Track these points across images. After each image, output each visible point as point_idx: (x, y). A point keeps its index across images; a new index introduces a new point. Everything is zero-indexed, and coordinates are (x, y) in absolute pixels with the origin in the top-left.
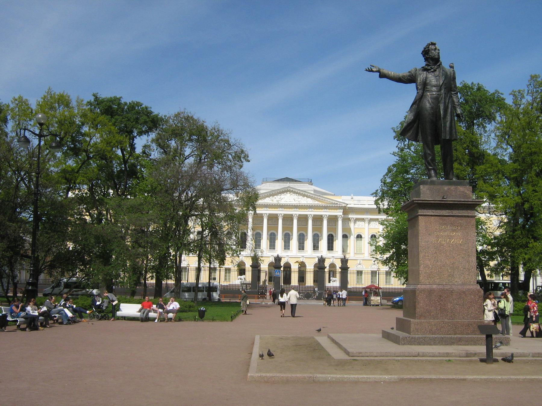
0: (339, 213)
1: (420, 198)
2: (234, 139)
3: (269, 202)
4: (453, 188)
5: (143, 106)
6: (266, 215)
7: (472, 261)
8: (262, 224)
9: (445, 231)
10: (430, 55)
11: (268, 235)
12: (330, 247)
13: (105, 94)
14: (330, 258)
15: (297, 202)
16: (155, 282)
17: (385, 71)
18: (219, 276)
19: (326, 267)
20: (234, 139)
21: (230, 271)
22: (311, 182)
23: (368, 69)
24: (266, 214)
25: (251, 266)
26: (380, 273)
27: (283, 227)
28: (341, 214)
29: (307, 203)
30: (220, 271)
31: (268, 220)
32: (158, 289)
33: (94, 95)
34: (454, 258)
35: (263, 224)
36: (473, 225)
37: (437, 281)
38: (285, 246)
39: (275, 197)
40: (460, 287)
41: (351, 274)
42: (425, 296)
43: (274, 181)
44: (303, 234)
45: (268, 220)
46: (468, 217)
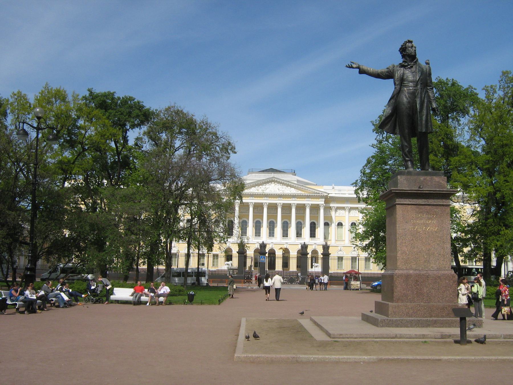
0: (321, 202)
1: (397, 187)
2: (222, 131)
3: (255, 191)
4: (428, 178)
5: (136, 100)
6: (251, 204)
7: (447, 248)
8: (248, 212)
9: (422, 219)
10: (407, 52)
11: (253, 223)
12: (313, 234)
13: (100, 89)
14: (312, 245)
15: (281, 192)
16: (146, 267)
17: (365, 67)
18: (207, 262)
19: (308, 253)
20: (222, 131)
21: (218, 257)
22: (294, 172)
23: (348, 66)
24: (252, 203)
25: (237, 252)
26: (359, 259)
27: (268, 216)
28: (323, 203)
29: (290, 192)
30: (208, 257)
31: (254, 208)
32: (149, 274)
33: (89, 90)
34: (429, 244)
35: (249, 213)
36: (448, 214)
37: (414, 267)
38: (270, 233)
39: (261, 186)
40: (435, 272)
41: (332, 260)
42: (402, 280)
43: (259, 172)
44: (287, 222)
45: (254, 209)
46: (443, 205)
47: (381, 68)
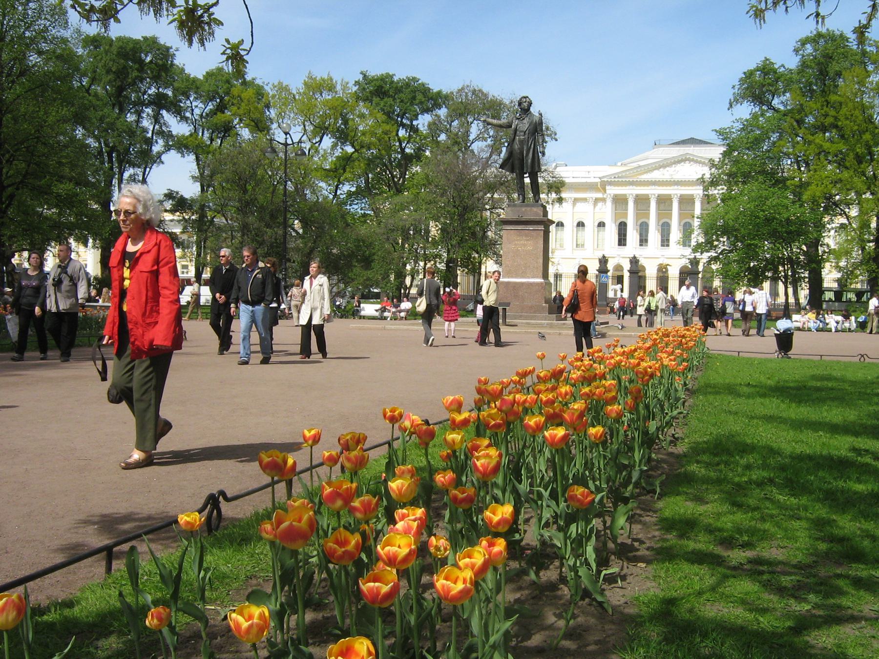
4: (529, 209)
5: (420, 82)
6: (653, 196)
13: (376, 71)
19: (609, 271)
24: (654, 195)
33: (362, 73)
38: (663, 241)
39: (668, 168)
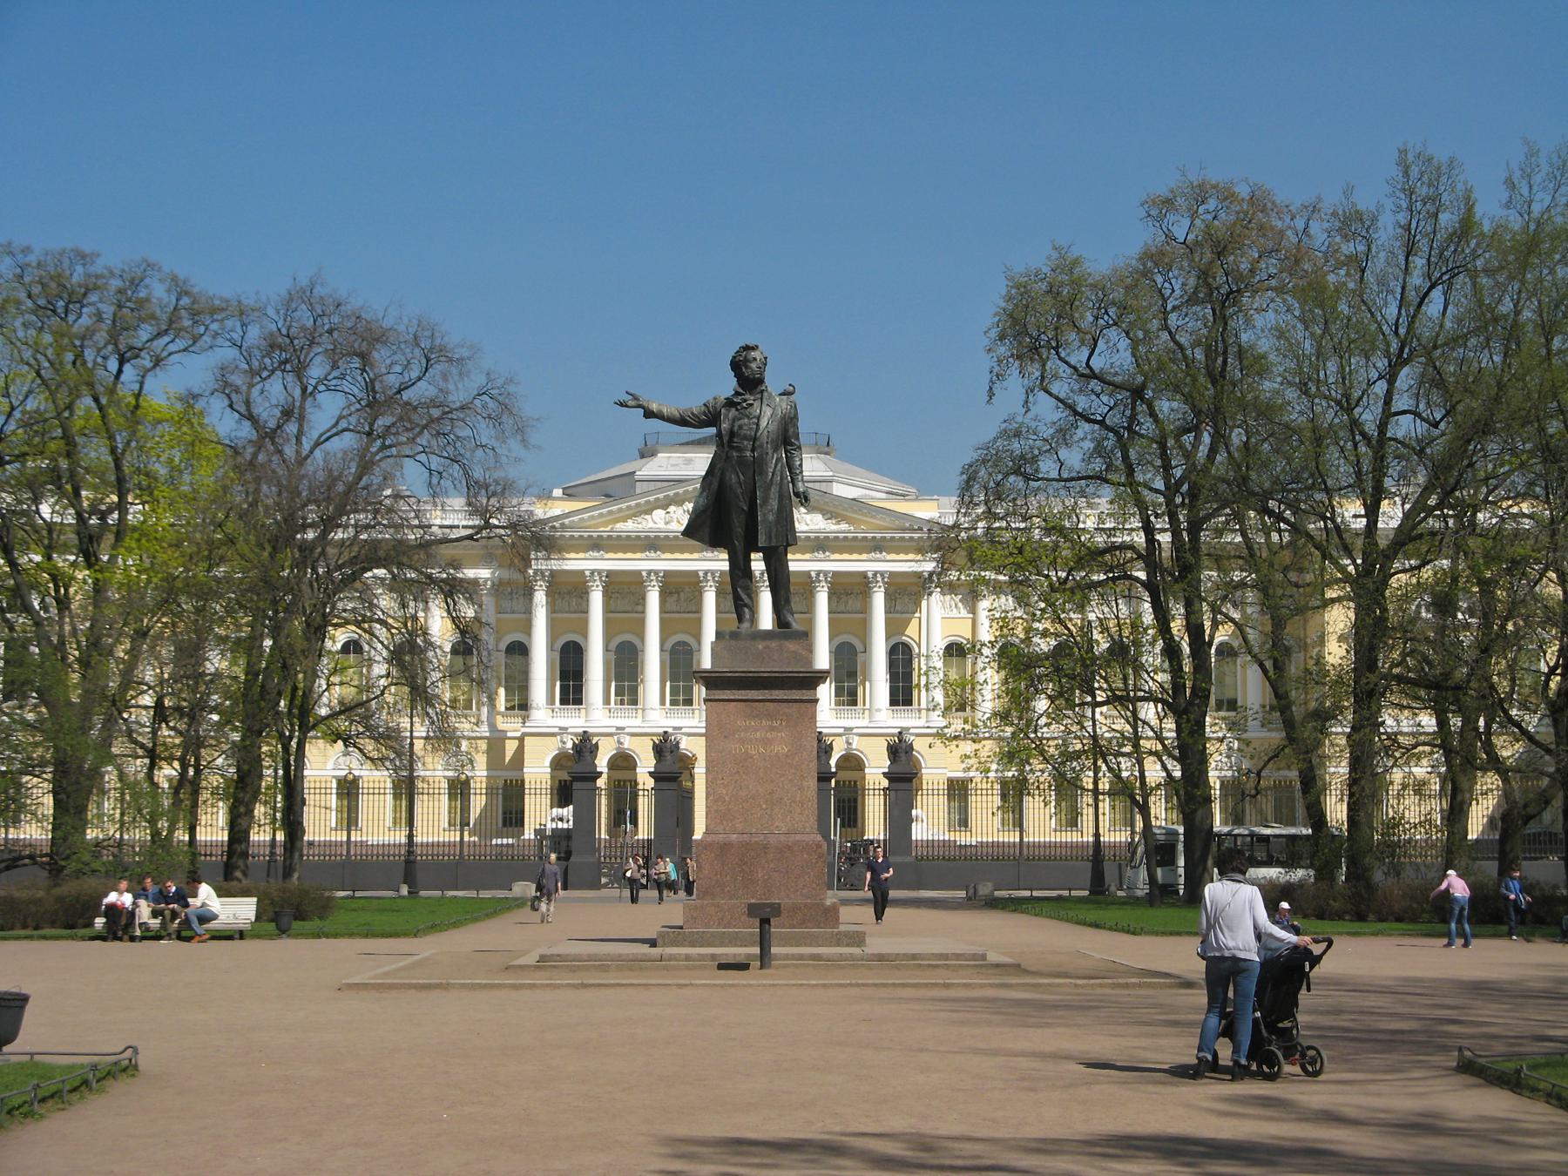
3: (662, 526)
8: (640, 608)
9: (756, 730)
11: (662, 650)
16: (226, 838)
17: (654, 407)
34: (773, 781)
37: (740, 827)
40: (782, 838)
43: (687, 444)
46: (802, 701)
47: (694, 403)
